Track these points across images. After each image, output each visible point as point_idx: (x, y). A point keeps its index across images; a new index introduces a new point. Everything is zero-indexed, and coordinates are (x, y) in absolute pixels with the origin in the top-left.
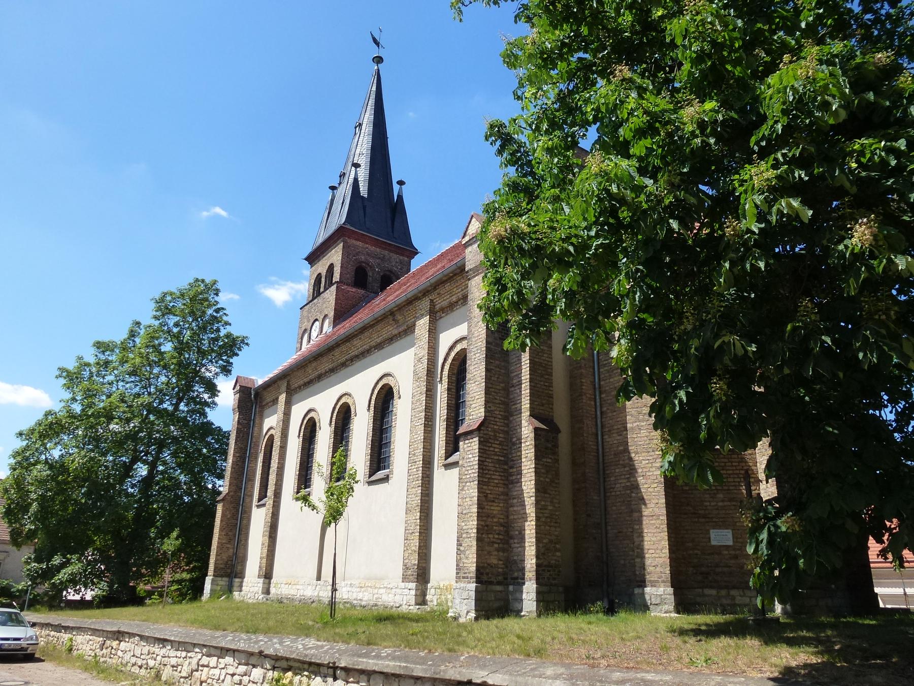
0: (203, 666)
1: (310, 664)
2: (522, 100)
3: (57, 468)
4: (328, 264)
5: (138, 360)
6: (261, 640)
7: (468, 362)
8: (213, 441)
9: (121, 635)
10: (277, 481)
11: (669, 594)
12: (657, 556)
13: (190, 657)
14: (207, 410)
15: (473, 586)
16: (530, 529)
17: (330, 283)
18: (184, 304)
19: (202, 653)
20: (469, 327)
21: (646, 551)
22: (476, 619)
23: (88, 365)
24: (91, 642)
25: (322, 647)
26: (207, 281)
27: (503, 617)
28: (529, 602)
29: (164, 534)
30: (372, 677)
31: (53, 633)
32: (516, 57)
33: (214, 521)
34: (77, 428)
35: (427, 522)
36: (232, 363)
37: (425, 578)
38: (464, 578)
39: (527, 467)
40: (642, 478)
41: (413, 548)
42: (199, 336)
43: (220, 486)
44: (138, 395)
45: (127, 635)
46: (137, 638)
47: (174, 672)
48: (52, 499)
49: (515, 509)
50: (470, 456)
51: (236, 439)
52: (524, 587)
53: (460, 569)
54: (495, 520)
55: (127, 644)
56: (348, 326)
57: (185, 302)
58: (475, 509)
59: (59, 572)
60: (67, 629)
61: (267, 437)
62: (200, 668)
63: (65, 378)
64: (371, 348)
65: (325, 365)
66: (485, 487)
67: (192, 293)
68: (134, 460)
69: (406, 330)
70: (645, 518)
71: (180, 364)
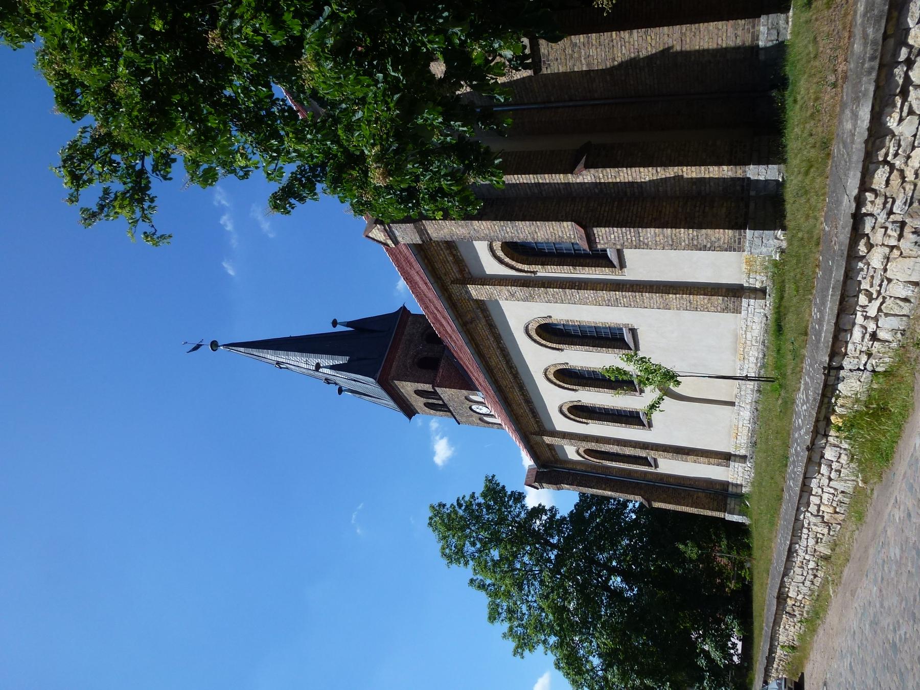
0: (818, 511)
1: (823, 395)
2: (249, 171)
3: (609, 658)
4: (415, 395)
5: (508, 581)
6: (796, 450)
7: (515, 240)
8: (589, 512)
9: (781, 596)
10: (631, 446)
11: (768, 20)
12: (725, 34)
13: (809, 524)
14: (558, 517)
15: (749, 233)
16: (691, 172)
17: (434, 394)
18: (454, 536)
19: (805, 512)
20: (479, 239)
21: (719, 47)
22: (784, 228)
23: (511, 629)
24: (787, 627)
25: (806, 384)
26: (431, 514)
27: (784, 201)
28: (769, 173)
29: (680, 559)
30: (841, 326)
31: (775, 666)
32: (206, 171)
33: (669, 510)
34: (573, 640)
35: (679, 287)
36: (512, 492)
37: (737, 290)
38: (739, 243)
39: (626, 176)
40: (640, 53)
41: (706, 301)
42: (484, 524)
43: (634, 506)
44: (542, 582)
45: (782, 590)
46: (786, 579)
47: (823, 541)
48: (641, 664)
49: (669, 189)
50: (612, 236)
51: (588, 487)
52: (752, 178)
53: (731, 247)
54: (680, 210)
55: (791, 590)
56: (477, 375)
57: (451, 536)
58: (668, 231)
59: (713, 660)
60: (772, 650)
61: (586, 456)
62: (821, 514)
63: (523, 650)
64: (499, 347)
65: (516, 395)
66: (645, 221)
67: (443, 529)
68: (606, 588)
69: (481, 310)
70: (683, 49)
71: (511, 542)
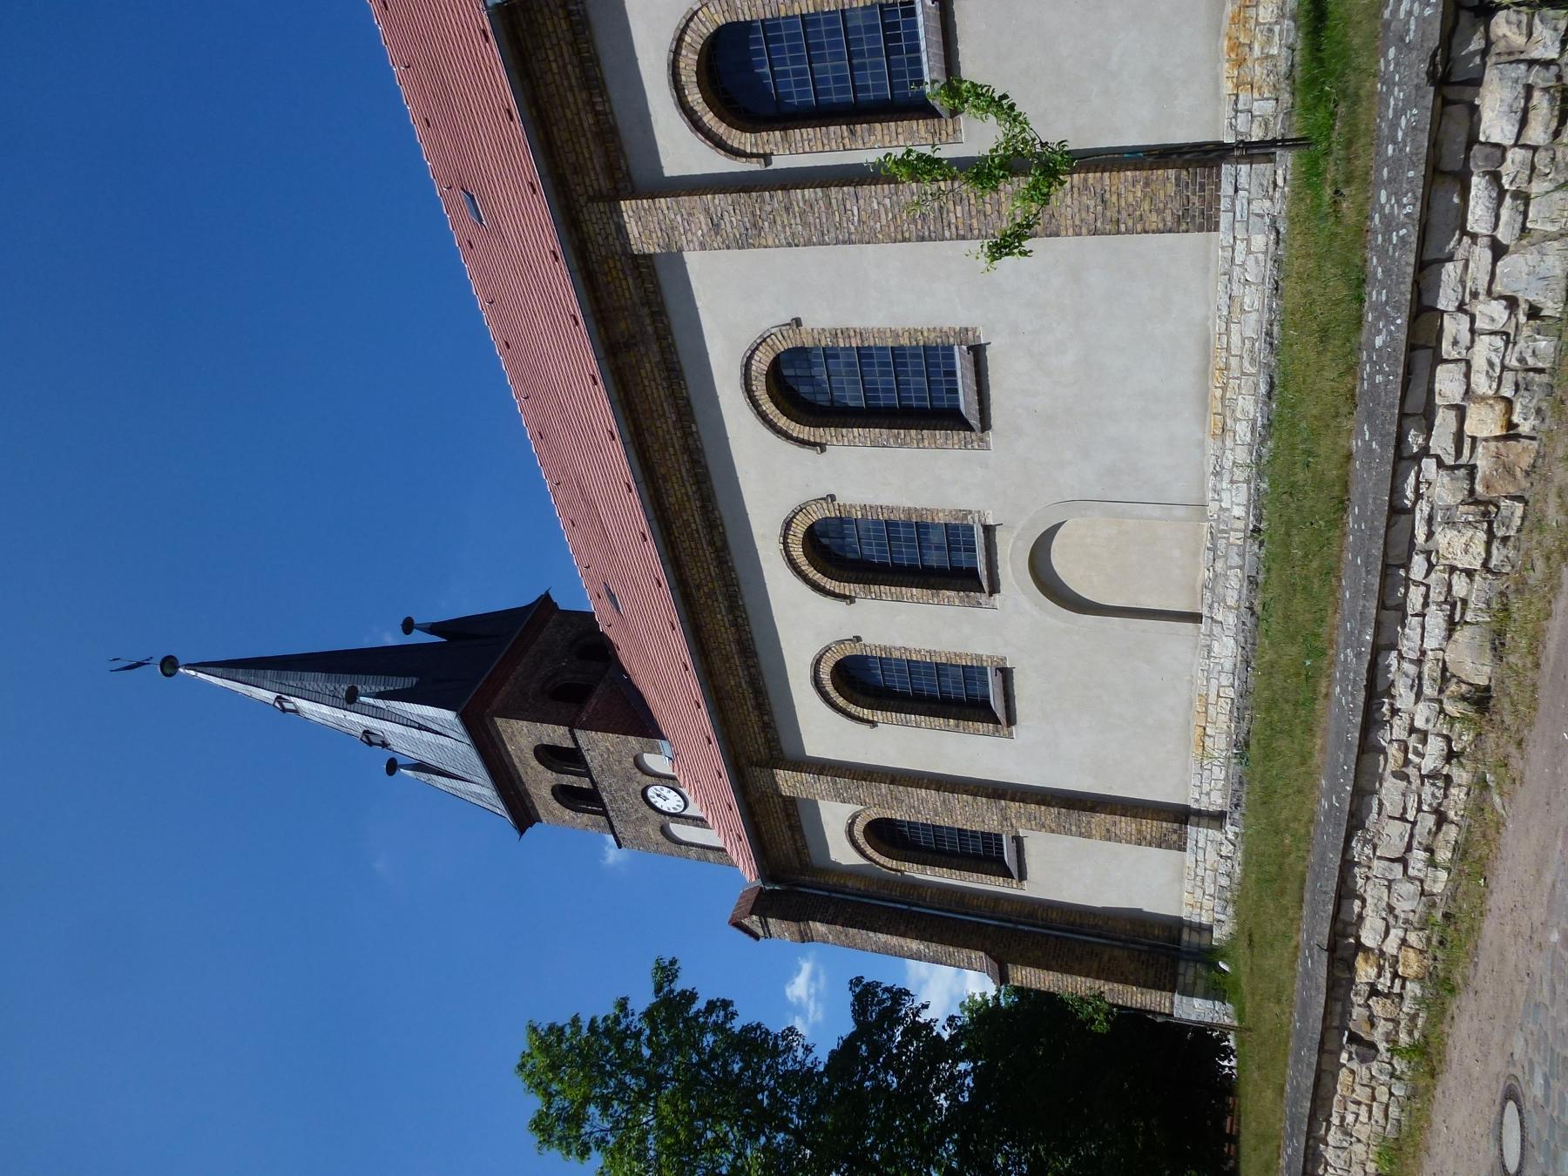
4: (535, 763)
10: (967, 792)
64: (687, 449)
